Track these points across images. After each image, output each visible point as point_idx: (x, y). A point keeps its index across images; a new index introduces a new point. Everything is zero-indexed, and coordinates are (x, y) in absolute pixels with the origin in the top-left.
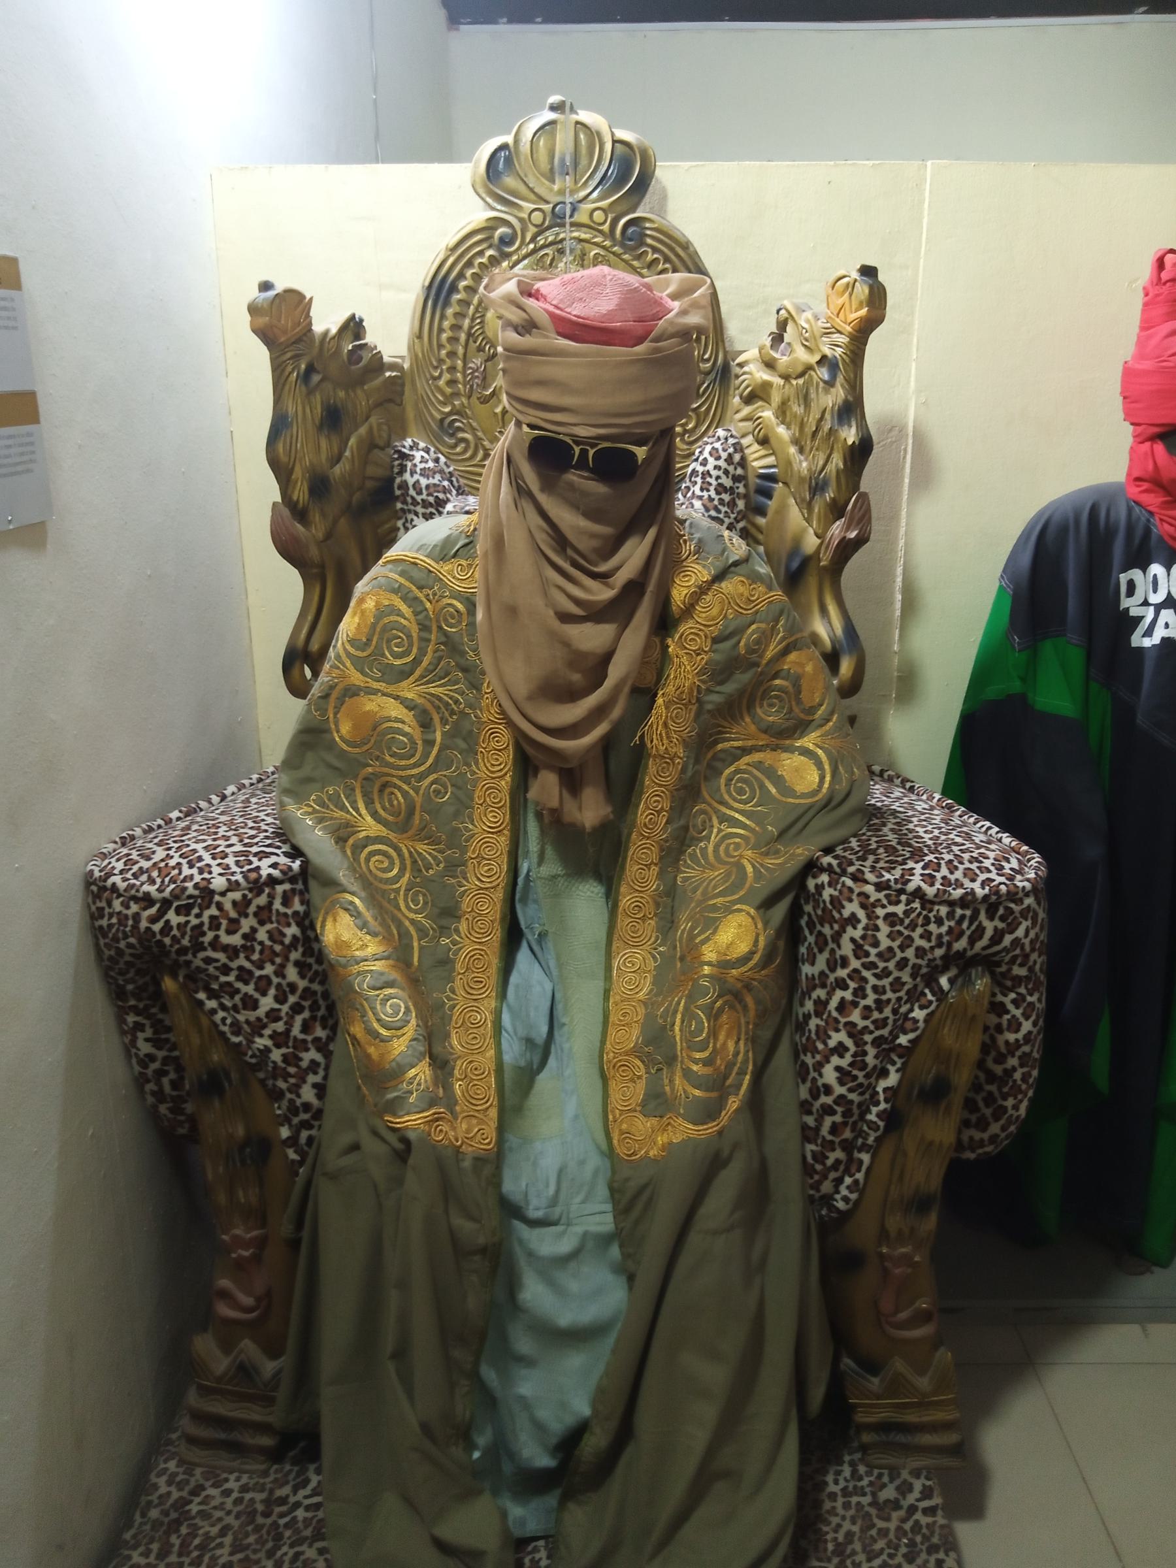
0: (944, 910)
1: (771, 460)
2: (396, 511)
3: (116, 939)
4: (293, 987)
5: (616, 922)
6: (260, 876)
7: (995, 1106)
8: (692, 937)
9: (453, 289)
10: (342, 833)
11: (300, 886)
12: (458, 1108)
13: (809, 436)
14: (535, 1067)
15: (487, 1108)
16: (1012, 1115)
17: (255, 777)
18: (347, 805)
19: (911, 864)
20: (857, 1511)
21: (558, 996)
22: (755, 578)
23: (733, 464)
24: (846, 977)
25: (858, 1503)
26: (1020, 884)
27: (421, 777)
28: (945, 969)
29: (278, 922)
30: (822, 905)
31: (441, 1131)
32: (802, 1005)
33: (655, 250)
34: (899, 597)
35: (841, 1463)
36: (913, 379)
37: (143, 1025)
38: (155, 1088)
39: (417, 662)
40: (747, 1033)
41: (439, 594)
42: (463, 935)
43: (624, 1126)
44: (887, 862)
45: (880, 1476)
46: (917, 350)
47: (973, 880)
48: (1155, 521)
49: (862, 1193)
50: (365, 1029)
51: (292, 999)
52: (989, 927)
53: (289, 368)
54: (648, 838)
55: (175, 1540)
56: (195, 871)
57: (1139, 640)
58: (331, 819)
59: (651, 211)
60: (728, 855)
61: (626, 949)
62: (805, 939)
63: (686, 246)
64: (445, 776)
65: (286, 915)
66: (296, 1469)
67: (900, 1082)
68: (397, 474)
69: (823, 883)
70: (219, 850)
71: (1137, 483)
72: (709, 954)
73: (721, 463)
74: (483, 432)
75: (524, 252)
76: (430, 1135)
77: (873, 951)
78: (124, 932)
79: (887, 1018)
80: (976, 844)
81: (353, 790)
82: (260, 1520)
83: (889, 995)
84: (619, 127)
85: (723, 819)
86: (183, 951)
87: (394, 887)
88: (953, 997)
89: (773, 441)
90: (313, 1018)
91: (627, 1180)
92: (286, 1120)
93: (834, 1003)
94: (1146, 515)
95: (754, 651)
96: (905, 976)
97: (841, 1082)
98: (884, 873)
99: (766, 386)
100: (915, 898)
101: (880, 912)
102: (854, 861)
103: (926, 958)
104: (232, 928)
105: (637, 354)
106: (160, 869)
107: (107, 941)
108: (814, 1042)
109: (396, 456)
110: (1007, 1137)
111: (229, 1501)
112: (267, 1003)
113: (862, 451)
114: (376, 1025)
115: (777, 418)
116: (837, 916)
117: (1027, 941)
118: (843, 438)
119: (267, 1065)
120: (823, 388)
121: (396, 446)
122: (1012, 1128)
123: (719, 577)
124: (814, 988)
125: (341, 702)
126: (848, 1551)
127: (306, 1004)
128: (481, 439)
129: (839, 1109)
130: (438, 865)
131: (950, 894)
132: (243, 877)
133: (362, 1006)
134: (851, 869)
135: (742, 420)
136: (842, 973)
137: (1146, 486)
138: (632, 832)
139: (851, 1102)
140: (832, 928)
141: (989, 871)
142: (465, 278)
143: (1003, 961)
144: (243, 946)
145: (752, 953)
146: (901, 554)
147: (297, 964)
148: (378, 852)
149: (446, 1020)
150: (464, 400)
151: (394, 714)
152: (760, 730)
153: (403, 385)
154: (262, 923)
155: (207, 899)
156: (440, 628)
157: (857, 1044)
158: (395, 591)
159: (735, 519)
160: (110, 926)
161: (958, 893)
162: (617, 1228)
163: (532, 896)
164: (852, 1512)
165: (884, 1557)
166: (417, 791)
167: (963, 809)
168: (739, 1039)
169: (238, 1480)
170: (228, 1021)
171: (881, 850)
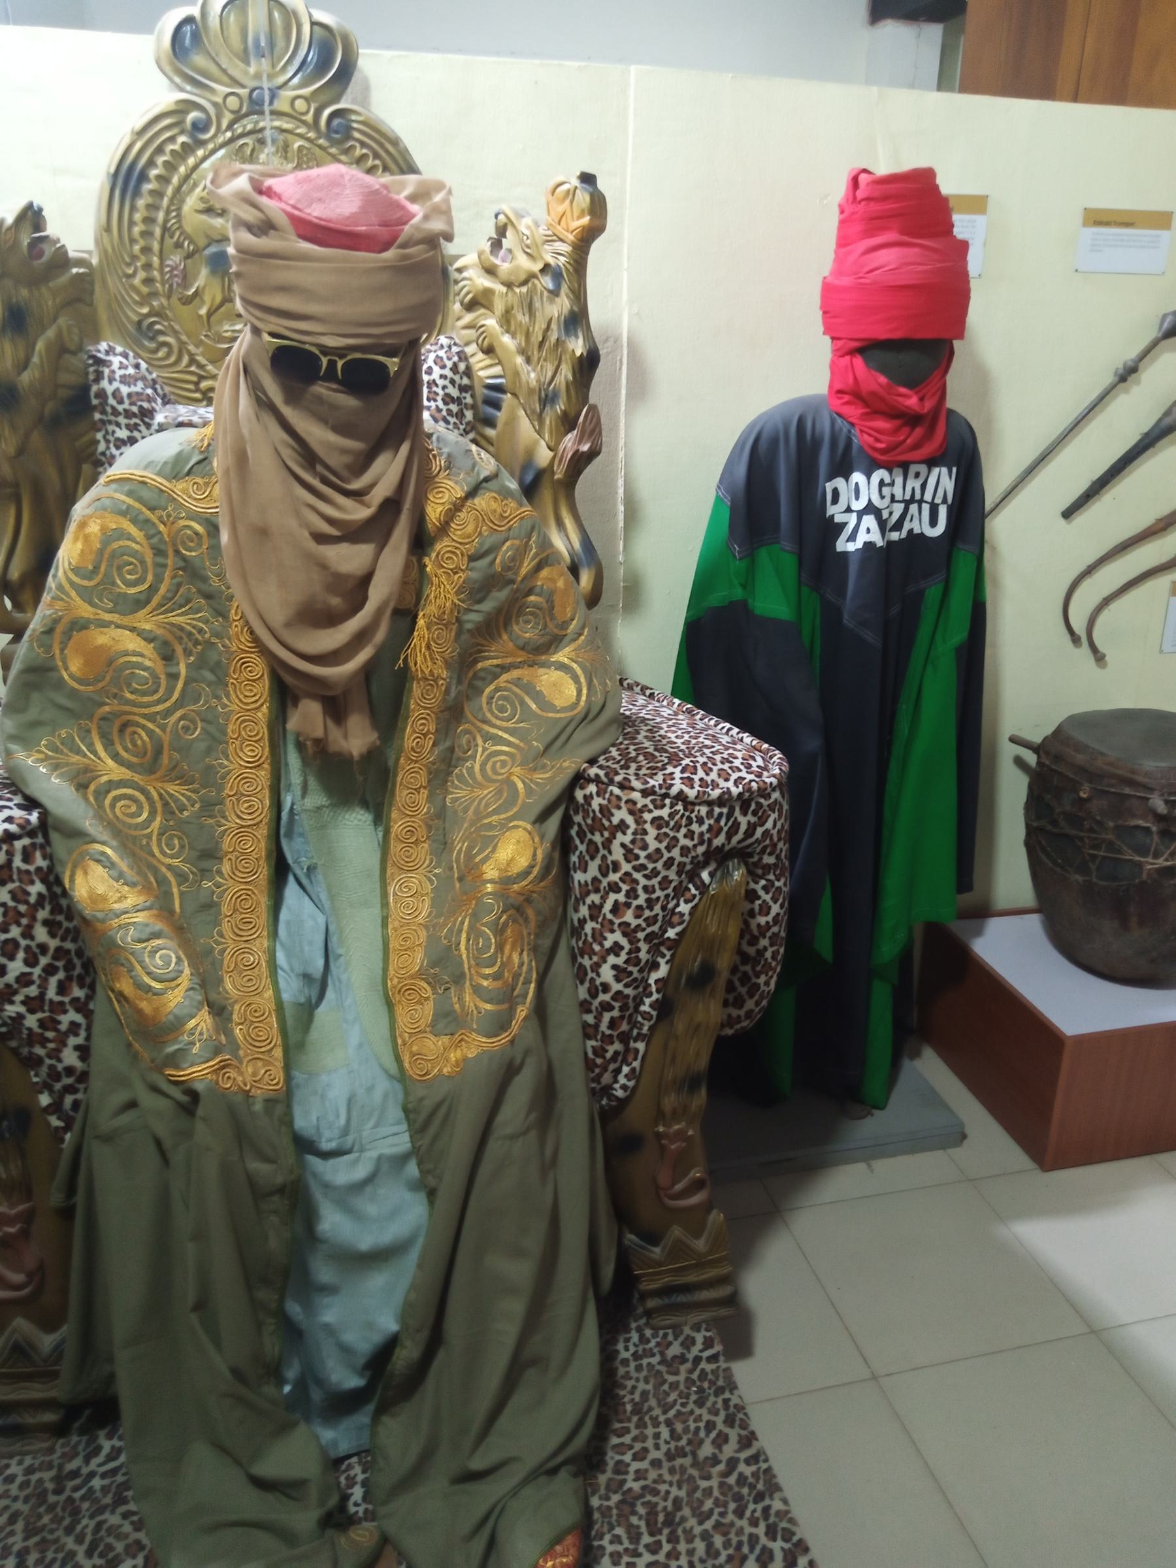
0: (704, 810)
1: (498, 370)
2: (94, 423)
4: (43, 948)
5: (389, 848)
7: (750, 984)
8: (469, 856)
9: (143, 177)
10: (83, 779)
11: (40, 840)
12: (241, 1053)
15: (272, 1049)
18: (84, 748)
19: (670, 769)
20: (649, 1371)
21: (331, 928)
22: (505, 493)
23: (458, 372)
24: (618, 881)
25: (649, 1364)
26: (768, 781)
27: (168, 713)
28: (705, 864)
29: (21, 881)
30: (591, 814)
31: (229, 1078)
32: (576, 910)
34: (622, 508)
35: (628, 1331)
39: (152, 589)
43: (415, 1048)
44: (648, 769)
45: (665, 1335)
47: (727, 780)
48: (855, 432)
50: (134, 984)
51: (44, 961)
52: (744, 821)
54: (416, 762)
57: (843, 545)
59: (354, 102)
62: (576, 848)
63: (396, 142)
64: (193, 711)
65: (28, 872)
66: (85, 1439)
71: (840, 395)
72: (490, 872)
73: (447, 372)
74: (189, 337)
75: (221, 139)
77: (643, 854)
79: (657, 915)
80: (724, 745)
81: (89, 731)
82: (52, 1498)
83: (659, 893)
85: (487, 737)
87: (146, 832)
88: (713, 890)
89: (498, 350)
90: (69, 978)
91: (422, 1099)
92: (47, 1087)
93: (608, 906)
95: (509, 569)
96: (672, 874)
98: (649, 780)
99: (488, 292)
102: (618, 769)
103: (690, 856)
105: (385, 261)
109: (91, 362)
111: (14, 1489)
113: (588, 364)
114: (147, 980)
115: (502, 327)
116: (606, 823)
117: (774, 832)
118: (570, 350)
119: (21, 1032)
121: (90, 351)
122: (764, 1003)
123: (472, 493)
124: (588, 893)
125: (68, 635)
126: (645, 1409)
128: (186, 343)
129: (617, 1005)
130: (193, 806)
131: (709, 795)
133: (128, 960)
134: (618, 779)
136: (614, 877)
137: (847, 398)
138: (400, 757)
139: (628, 996)
140: (602, 835)
141: (740, 770)
145: (532, 867)
146: (621, 466)
147: (46, 923)
148: (117, 799)
149: (216, 965)
150: (164, 301)
153: (92, 283)
156: (177, 552)
157: (630, 942)
158: (123, 514)
159: (464, 430)
161: (715, 794)
162: (413, 1146)
163: (297, 829)
164: (645, 1373)
165: (678, 1407)
166: (163, 729)
167: (702, 712)
168: (522, 951)
169: (20, 1463)
171: (641, 758)
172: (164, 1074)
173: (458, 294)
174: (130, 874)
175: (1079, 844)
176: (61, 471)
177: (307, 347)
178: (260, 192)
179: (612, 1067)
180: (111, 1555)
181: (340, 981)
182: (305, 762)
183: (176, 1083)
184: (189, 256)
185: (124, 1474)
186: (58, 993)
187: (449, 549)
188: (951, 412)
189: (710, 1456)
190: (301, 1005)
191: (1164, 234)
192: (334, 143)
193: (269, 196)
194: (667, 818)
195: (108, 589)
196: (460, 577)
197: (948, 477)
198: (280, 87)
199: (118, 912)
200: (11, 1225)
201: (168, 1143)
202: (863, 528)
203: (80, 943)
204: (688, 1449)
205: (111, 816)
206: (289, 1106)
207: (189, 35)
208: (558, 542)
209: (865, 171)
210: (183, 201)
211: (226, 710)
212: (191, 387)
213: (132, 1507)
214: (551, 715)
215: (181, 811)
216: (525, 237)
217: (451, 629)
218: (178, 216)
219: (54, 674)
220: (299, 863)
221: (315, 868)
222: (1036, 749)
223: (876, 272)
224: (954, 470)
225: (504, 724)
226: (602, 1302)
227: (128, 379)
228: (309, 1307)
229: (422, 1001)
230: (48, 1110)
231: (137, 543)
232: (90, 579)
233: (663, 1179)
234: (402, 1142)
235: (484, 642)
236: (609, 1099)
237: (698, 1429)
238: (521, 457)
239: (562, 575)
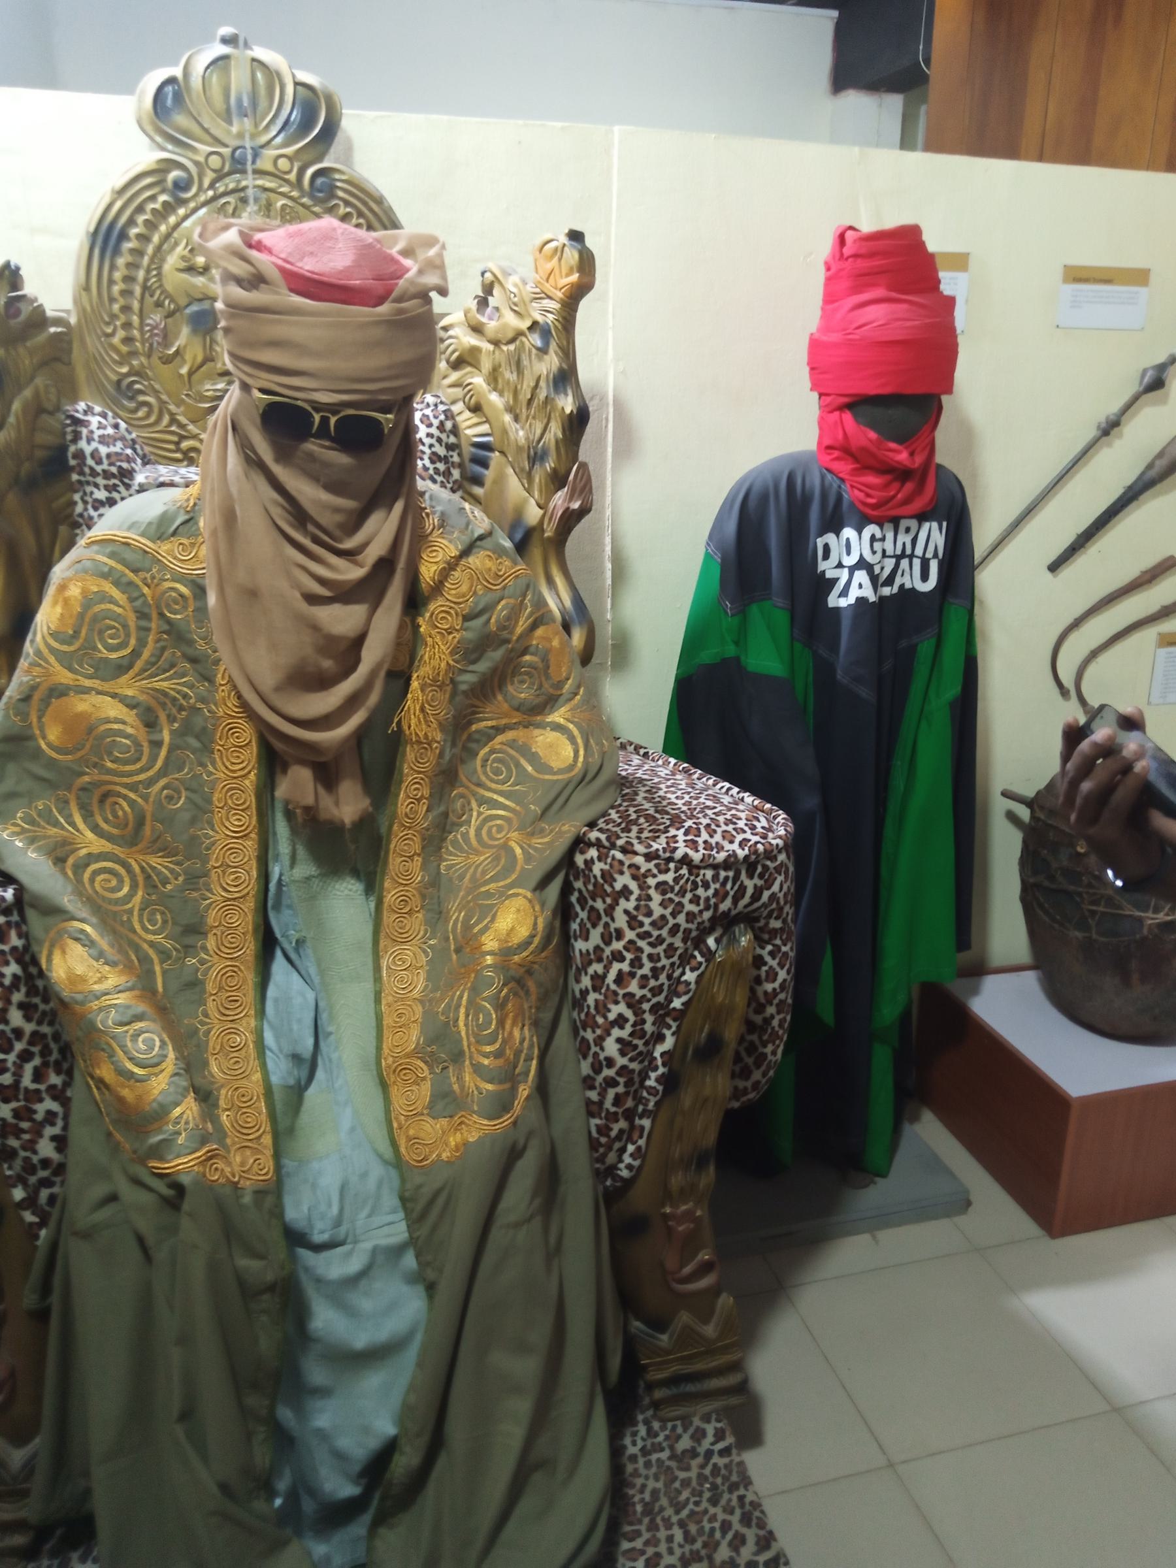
0: (709, 874)
1: (485, 428)
2: (72, 483)
8: (467, 927)
9: (123, 236)
10: (60, 853)
11: (15, 917)
16: (771, 1061)
18: (62, 820)
19: (673, 832)
20: (658, 1467)
21: (322, 1004)
22: (500, 552)
23: (445, 431)
24: (622, 949)
25: (658, 1460)
26: (774, 842)
27: (151, 782)
28: (710, 931)
30: (593, 880)
32: (578, 981)
33: (347, 203)
34: (609, 566)
35: (635, 1424)
39: (135, 654)
40: (530, 1018)
42: (211, 953)
43: (411, 1132)
44: (650, 831)
45: (674, 1428)
46: (614, 317)
47: (731, 842)
48: (846, 487)
50: (116, 1070)
51: (19, 1046)
52: (750, 885)
54: (410, 828)
57: (835, 601)
59: (337, 161)
60: (492, 838)
61: (395, 946)
62: (577, 915)
63: (380, 201)
64: (177, 779)
69: (592, 858)
72: (490, 943)
73: (434, 430)
74: (169, 395)
75: (202, 198)
77: (647, 921)
79: (663, 984)
80: (726, 806)
81: (67, 802)
83: (664, 961)
85: (482, 801)
88: (720, 956)
89: (485, 408)
90: (45, 1064)
91: (420, 1186)
92: (21, 1180)
94: (838, 481)
95: (504, 628)
96: (678, 942)
97: (623, 1053)
98: (652, 843)
99: (475, 351)
100: (683, 864)
102: (619, 832)
103: (696, 922)
105: (379, 315)
109: (68, 422)
110: (766, 1082)
113: (578, 422)
114: (129, 1066)
115: (489, 385)
116: (609, 889)
117: (781, 895)
121: (68, 411)
122: (771, 1073)
123: (466, 552)
124: (590, 963)
125: (46, 702)
126: (657, 1509)
129: (621, 1080)
130: (176, 879)
131: (714, 858)
134: (620, 842)
136: (618, 945)
137: (836, 453)
139: (633, 1071)
140: (604, 902)
141: (744, 832)
143: (761, 916)
145: (532, 936)
146: (608, 523)
147: (21, 1006)
148: (96, 873)
149: (202, 1047)
150: (143, 359)
151: (112, 713)
153: (70, 343)
156: (161, 615)
157: (635, 1014)
158: (104, 576)
161: (721, 857)
162: (411, 1237)
163: (285, 901)
164: (654, 1470)
165: (691, 1506)
166: (145, 798)
167: (700, 772)
168: (523, 1026)
171: (642, 820)
173: (444, 353)
175: (1078, 899)
176: (37, 532)
177: (299, 403)
178: (250, 246)
181: (330, 1060)
182: (294, 831)
184: (170, 315)
188: (939, 467)
189: (727, 1559)
190: (291, 1087)
191: (1143, 291)
192: (318, 201)
193: (259, 250)
194: (671, 883)
196: (454, 637)
197: (938, 532)
198: (263, 147)
199: (98, 993)
201: (150, 1241)
202: (855, 584)
203: (57, 1026)
204: (703, 1552)
205: (90, 891)
207: (170, 96)
209: (851, 228)
210: (163, 260)
211: (212, 777)
212: (172, 447)
214: (547, 777)
216: (512, 295)
217: (445, 691)
218: (159, 275)
219: (31, 744)
220: (287, 937)
222: (1029, 803)
223: (865, 328)
224: (945, 524)
225: (500, 787)
226: (608, 1395)
227: (107, 440)
228: (299, 1410)
229: (418, 1081)
230: (22, 1205)
231: (120, 606)
232: (70, 644)
234: (396, 1231)
236: (614, 1180)
237: (713, 1530)
239: (557, 634)
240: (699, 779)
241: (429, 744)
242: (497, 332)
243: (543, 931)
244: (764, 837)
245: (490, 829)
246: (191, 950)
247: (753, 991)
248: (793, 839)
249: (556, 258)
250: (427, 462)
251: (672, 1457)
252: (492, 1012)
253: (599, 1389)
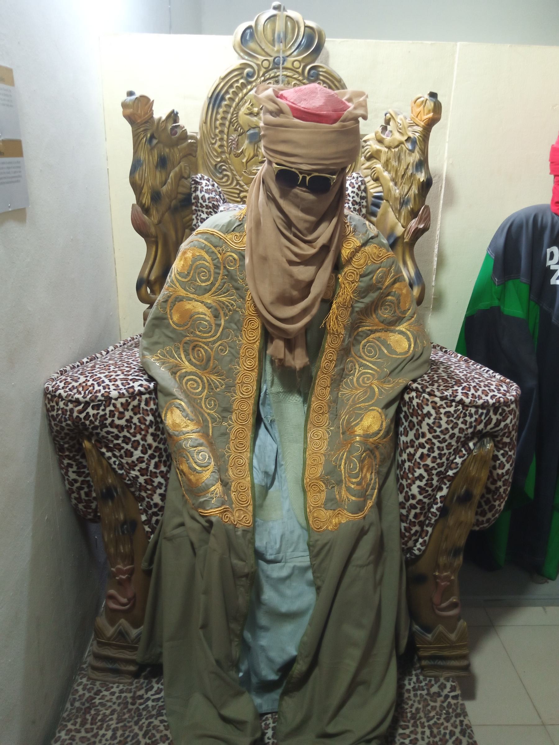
0: (473, 410)
1: (380, 189)
3: (60, 422)
4: (150, 446)
6: (135, 391)
7: (490, 505)
8: (349, 422)
9: (223, 99)
10: (174, 370)
11: (153, 396)
12: (234, 506)
13: (400, 177)
14: (268, 486)
15: (248, 506)
16: (497, 509)
17: (122, 342)
19: (456, 388)
20: (421, 698)
21: (279, 451)
22: (381, 245)
23: (360, 190)
24: (424, 442)
25: (421, 694)
26: (509, 398)
27: (214, 342)
28: (471, 439)
29: (143, 414)
30: (412, 407)
32: (401, 456)
34: (436, 259)
35: (411, 675)
36: (446, 151)
37: (72, 465)
38: (77, 496)
39: (213, 284)
40: (375, 470)
41: (225, 250)
42: (234, 421)
43: (315, 515)
44: (444, 386)
45: (430, 681)
46: (449, 137)
49: (427, 546)
50: (189, 467)
51: (150, 452)
52: (494, 418)
53: (142, 136)
54: (326, 374)
55: (89, 717)
56: (101, 388)
58: (168, 363)
59: (321, 62)
62: (403, 424)
64: (225, 342)
65: (147, 410)
66: (146, 681)
67: (448, 493)
68: (193, 192)
70: (112, 377)
72: (359, 431)
73: (355, 190)
76: (222, 519)
77: (438, 430)
78: (65, 418)
79: (444, 462)
81: (179, 348)
82: (130, 707)
83: (445, 451)
84: (309, 19)
85: (361, 365)
86: (96, 428)
88: (475, 452)
90: (160, 461)
91: (317, 541)
92: (145, 511)
95: (380, 282)
96: (453, 442)
97: (420, 493)
99: (378, 152)
101: (442, 411)
103: (464, 433)
104: (122, 416)
105: (334, 128)
106: (83, 387)
107: (56, 422)
108: (407, 474)
109: (193, 182)
111: (114, 698)
112: (137, 454)
113: (426, 185)
115: (384, 168)
116: (420, 412)
117: (511, 425)
118: (418, 178)
119: (137, 485)
120: (408, 153)
121: (193, 178)
122: (497, 515)
123: (364, 244)
124: (408, 447)
126: (418, 717)
127: (157, 454)
128: (235, 175)
129: (419, 506)
130: (222, 386)
131: (477, 402)
132: (126, 391)
133: (187, 455)
134: (428, 390)
135: (365, 169)
136: (422, 440)
138: (318, 371)
139: (425, 503)
140: (417, 418)
141: (494, 391)
142: (229, 94)
143: (499, 435)
144: (126, 425)
145: (380, 430)
147: (152, 434)
149: (226, 462)
151: (201, 310)
152: (380, 321)
153: (197, 147)
154: (135, 414)
155: (108, 402)
156: (225, 267)
157: (429, 475)
158: (203, 248)
160: (58, 415)
161: (480, 402)
162: (311, 564)
163: (267, 402)
164: (418, 698)
165: (435, 720)
167: (473, 361)
170: (117, 463)
171: (440, 381)
172: (198, 511)
174: (191, 415)
177: (293, 170)
178: (277, 97)
179: (414, 538)
180: (154, 739)
181: (281, 477)
182: (274, 370)
183: (203, 516)
185: (162, 702)
186: (154, 468)
187: (351, 271)
190: (263, 486)
193: (281, 99)
195: (193, 283)
196: (355, 285)
198: (288, 56)
199: (184, 432)
200: (124, 575)
201: (196, 545)
203: (166, 446)
205: (185, 388)
206: (253, 534)
208: (405, 274)
210: (239, 110)
212: (236, 195)
213: (165, 718)
214: (394, 356)
215: (216, 388)
216: (399, 124)
217: (348, 310)
219: (165, 321)
221: (274, 421)
229: (320, 491)
230: (144, 523)
231: (208, 262)
233: (436, 599)
234: (306, 561)
235: (364, 318)
237: (445, 734)
238: (388, 232)
240: (473, 365)
241: (338, 335)
242: (390, 142)
243: (385, 429)
244: (505, 395)
245: (364, 378)
246: (225, 419)
247: (491, 472)
248: (519, 398)
249: (422, 106)
250: (350, 205)
251: (428, 694)
252: (357, 463)
253: (394, 652)
